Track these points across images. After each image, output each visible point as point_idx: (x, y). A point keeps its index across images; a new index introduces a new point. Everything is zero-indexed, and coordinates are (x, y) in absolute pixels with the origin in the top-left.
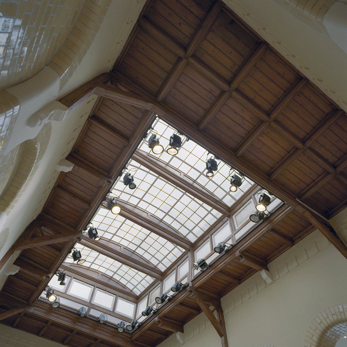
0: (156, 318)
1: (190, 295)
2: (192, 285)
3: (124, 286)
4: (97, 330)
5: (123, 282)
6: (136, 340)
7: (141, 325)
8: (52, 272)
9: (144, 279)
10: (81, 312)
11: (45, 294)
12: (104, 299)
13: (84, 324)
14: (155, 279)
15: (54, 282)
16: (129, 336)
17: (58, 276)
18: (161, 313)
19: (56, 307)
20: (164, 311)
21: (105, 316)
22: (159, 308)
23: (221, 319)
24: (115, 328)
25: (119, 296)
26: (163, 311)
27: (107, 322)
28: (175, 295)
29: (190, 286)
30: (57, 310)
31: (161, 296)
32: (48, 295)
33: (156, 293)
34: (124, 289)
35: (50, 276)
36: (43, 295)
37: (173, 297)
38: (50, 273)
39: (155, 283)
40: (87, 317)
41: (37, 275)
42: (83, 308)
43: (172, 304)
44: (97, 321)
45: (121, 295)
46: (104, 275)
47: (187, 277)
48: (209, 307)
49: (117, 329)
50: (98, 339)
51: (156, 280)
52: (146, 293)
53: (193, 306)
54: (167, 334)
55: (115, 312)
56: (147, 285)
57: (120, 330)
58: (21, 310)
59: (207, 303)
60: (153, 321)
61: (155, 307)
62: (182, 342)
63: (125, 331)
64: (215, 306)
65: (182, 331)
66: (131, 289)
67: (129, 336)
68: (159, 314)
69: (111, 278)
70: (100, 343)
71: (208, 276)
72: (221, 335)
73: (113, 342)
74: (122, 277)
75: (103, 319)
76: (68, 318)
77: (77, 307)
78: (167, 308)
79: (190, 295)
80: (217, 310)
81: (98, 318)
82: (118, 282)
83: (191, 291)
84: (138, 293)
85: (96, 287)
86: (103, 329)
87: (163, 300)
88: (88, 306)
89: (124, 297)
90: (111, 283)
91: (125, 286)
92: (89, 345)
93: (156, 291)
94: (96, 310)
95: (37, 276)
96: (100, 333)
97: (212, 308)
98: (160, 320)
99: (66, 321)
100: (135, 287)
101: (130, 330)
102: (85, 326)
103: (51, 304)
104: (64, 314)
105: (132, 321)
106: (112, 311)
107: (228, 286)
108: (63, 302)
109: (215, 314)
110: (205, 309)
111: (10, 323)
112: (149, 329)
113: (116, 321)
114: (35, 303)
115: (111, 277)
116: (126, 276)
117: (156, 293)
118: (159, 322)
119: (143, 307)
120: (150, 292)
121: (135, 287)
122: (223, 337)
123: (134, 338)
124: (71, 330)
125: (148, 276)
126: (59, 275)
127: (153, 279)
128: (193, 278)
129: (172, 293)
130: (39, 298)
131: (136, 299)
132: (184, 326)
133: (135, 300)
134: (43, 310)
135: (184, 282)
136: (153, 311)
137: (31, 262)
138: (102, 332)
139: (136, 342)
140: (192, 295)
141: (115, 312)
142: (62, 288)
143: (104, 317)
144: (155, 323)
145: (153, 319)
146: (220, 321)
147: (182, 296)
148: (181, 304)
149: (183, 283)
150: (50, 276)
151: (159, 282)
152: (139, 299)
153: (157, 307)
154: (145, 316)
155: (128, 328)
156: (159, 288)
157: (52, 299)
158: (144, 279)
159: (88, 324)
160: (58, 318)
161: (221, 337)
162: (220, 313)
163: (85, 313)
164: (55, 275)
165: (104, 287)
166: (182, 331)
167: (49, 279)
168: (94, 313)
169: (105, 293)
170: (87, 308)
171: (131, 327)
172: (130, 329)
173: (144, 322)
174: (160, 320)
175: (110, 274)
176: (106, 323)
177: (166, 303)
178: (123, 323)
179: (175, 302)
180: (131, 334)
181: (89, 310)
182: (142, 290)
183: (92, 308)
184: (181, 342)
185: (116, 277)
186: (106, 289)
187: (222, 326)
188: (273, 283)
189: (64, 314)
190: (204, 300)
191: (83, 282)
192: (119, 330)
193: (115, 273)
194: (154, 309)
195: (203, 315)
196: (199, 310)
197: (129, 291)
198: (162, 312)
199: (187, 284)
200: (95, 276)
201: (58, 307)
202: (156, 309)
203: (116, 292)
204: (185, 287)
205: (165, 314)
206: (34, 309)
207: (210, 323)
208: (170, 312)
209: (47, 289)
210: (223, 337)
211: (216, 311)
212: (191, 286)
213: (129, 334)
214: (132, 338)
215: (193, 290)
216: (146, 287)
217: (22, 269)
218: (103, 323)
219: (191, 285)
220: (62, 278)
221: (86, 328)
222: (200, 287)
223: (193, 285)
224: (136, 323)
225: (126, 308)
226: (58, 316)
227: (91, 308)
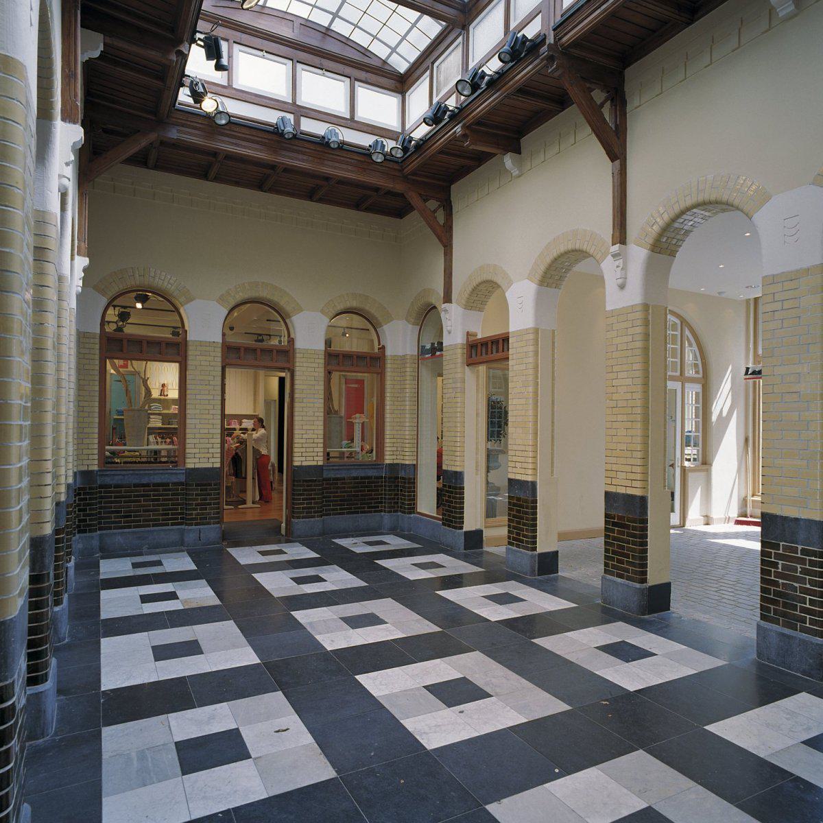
0: (458, 129)
1: (546, 66)
2: (555, 38)
3: (365, 52)
4: (326, 162)
5: (360, 38)
6: (414, 173)
7: (422, 144)
8: (185, 38)
9: (414, 25)
10: (282, 128)
11: (188, 96)
12: (324, 92)
13: (298, 152)
14: (444, 23)
15: (198, 64)
16: (396, 167)
17: (201, 46)
18: (468, 116)
19: (223, 122)
20: (475, 113)
21: (337, 131)
22: (464, 106)
23: (618, 123)
24: (364, 154)
25: (356, 80)
26: (472, 112)
27: (343, 143)
28: (505, 69)
29: (550, 44)
30: (228, 128)
31: (468, 77)
32: (198, 97)
33: (450, 68)
34: (366, 60)
35: (183, 49)
36: (184, 96)
37: (500, 75)
38: (181, 42)
39: (446, 36)
40: (297, 136)
41: (153, 53)
42: (283, 119)
43: (498, 94)
44: (322, 144)
45: (363, 75)
46: (307, 25)
47: (540, 15)
48: (591, 91)
49: (370, 155)
50: (331, 178)
51: (446, 28)
52: (424, 66)
53: (552, 94)
54: (480, 159)
55: (356, 119)
56: (424, 44)
57: (377, 158)
58: (153, 137)
59: (588, 85)
60: (451, 135)
61: (452, 103)
62: (517, 172)
63: (388, 157)
64: (608, 92)
65: (518, 151)
66: (383, 59)
67: (396, 167)
68: (465, 118)
69: (327, 32)
70: (337, 183)
71: (605, 10)
72: (613, 156)
73: (365, 182)
74: (375, 37)
75: (334, 139)
76: (257, 142)
77: (270, 116)
78: (481, 104)
79: (546, 66)
80: (612, 100)
81: (323, 138)
82: (346, 41)
83: (550, 59)
84: (402, 67)
85: (298, 62)
86: (338, 158)
87: (475, 86)
88: (293, 113)
89: (370, 81)
90: (332, 47)
91: (366, 49)
92: (314, 188)
93: (451, 58)
94: (313, 119)
95: (153, 54)
96: (335, 168)
97: (598, 96)
98: (467, 132)
99: (256, 150)
100: (394, 50)
101: (399, 156)
102: (300, 157)
103: (208, 117)
104: (247, 136)
105: (401, 136)
106: (349, 117)
107: (654, 31)
108: (235, 108)
109: (607, 112)
110: (583, 102)
111: (141, 160)
112: (441, 152)
113: (365, 140)
114: (174, 118)
115: (328, 29)
116: (366, 23)
117: (450, 68)
118: (464, 136)
119: (419, 101)
120: (433, 63)
121: (394, 50)
122: (619, 160)
123: (408, 170)
124: (273, 167)
125: (426, 18)
126: (202, 44)
127: (441, 24)
128: (558, 19)
129: (494, 65)
130: (177, 104)
131: (400, 83)
132: (523, 140)
133: (398, 85)
134: (197, 132)
135: (531, 32)
136: (448, 113)
137: (117, 14)
138: (337, 165)
139: (414, 178)
140: (554, 69)
141: (356, 119)
142: (219, 77)
143: (336, 134)
144: (454, 138)
145: (452, 129)
146: (616, 126)
147: (526, 72)
148: (523, 91)
149: (530, 37)
150: (183, 49)
151: (458, 31)
152: (405, 81)
153: (457, 103)
154: (432, 125)
155: (393, 153)
156: (460, 49)
157: (208, 105)
158: (414, 25)
159: (305, 152)
160: (236, 145)
161: (612, 161)
162: (618, 108)
163: (291, 130)
164: (194, 46)
165: (317, 60)
166: (518, 151)
167: (184, 58)
168: (310, 126)
169: (263, 57)
170: (290, 117)
171: (400, 150)
172: (399, 154)
173: (428, 137)
174: (467, 132)
175: (323, 20)
176: (342, 146)
177: (483, 92)
178: (380, 142)
179: (504, 88)
180: (402, 162)
181: (297, 123)
182: (413, 56)
183: (303, 116)
184: (515, 172)
185: (340, 27)
186: (322, 65)
187: (618, 138)
188: (796, 15)
189: (247, 136)
190: (582, 77)
191: (262, 51)
192: (374, 157)
193: (335, 15)
194: (451, 108)
195: (573, 112)
196: (562, 102)
197: (379, 64)
198: (470, 114)
199: (539, 40)
200: (285, 31)
201: (230, 122)
202: (456, 108)
203: (348, 70)
204: (539, 41)
205: (480, 117)
206: (179, 131)
207: (589, 130)
208: (492, 112)
209: (187, 81)
210: (617, 162)
211: (608, 104)
212: (552, 42)
213: (397, 162)
214: (403, 170)
215: (556, 55)
216: (422, 48)
217: (109, 40)
218: (336, 146)
219: (551, 40)
220: (213, 51)
221: (303, 161)
222: (576, 44)
223: (558, 39)
224: (410, 142)
225: (378, 107)
226: (234, 141)
227: (302, 116)
